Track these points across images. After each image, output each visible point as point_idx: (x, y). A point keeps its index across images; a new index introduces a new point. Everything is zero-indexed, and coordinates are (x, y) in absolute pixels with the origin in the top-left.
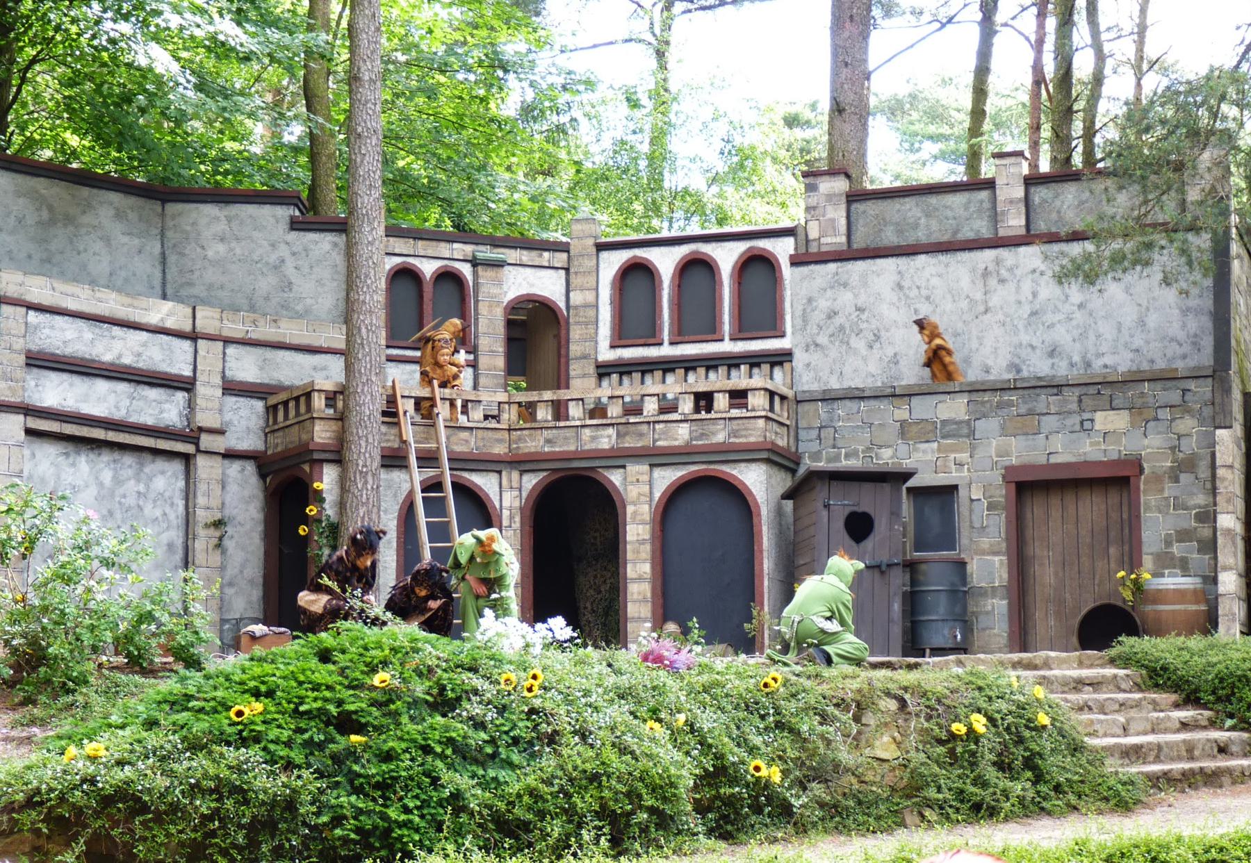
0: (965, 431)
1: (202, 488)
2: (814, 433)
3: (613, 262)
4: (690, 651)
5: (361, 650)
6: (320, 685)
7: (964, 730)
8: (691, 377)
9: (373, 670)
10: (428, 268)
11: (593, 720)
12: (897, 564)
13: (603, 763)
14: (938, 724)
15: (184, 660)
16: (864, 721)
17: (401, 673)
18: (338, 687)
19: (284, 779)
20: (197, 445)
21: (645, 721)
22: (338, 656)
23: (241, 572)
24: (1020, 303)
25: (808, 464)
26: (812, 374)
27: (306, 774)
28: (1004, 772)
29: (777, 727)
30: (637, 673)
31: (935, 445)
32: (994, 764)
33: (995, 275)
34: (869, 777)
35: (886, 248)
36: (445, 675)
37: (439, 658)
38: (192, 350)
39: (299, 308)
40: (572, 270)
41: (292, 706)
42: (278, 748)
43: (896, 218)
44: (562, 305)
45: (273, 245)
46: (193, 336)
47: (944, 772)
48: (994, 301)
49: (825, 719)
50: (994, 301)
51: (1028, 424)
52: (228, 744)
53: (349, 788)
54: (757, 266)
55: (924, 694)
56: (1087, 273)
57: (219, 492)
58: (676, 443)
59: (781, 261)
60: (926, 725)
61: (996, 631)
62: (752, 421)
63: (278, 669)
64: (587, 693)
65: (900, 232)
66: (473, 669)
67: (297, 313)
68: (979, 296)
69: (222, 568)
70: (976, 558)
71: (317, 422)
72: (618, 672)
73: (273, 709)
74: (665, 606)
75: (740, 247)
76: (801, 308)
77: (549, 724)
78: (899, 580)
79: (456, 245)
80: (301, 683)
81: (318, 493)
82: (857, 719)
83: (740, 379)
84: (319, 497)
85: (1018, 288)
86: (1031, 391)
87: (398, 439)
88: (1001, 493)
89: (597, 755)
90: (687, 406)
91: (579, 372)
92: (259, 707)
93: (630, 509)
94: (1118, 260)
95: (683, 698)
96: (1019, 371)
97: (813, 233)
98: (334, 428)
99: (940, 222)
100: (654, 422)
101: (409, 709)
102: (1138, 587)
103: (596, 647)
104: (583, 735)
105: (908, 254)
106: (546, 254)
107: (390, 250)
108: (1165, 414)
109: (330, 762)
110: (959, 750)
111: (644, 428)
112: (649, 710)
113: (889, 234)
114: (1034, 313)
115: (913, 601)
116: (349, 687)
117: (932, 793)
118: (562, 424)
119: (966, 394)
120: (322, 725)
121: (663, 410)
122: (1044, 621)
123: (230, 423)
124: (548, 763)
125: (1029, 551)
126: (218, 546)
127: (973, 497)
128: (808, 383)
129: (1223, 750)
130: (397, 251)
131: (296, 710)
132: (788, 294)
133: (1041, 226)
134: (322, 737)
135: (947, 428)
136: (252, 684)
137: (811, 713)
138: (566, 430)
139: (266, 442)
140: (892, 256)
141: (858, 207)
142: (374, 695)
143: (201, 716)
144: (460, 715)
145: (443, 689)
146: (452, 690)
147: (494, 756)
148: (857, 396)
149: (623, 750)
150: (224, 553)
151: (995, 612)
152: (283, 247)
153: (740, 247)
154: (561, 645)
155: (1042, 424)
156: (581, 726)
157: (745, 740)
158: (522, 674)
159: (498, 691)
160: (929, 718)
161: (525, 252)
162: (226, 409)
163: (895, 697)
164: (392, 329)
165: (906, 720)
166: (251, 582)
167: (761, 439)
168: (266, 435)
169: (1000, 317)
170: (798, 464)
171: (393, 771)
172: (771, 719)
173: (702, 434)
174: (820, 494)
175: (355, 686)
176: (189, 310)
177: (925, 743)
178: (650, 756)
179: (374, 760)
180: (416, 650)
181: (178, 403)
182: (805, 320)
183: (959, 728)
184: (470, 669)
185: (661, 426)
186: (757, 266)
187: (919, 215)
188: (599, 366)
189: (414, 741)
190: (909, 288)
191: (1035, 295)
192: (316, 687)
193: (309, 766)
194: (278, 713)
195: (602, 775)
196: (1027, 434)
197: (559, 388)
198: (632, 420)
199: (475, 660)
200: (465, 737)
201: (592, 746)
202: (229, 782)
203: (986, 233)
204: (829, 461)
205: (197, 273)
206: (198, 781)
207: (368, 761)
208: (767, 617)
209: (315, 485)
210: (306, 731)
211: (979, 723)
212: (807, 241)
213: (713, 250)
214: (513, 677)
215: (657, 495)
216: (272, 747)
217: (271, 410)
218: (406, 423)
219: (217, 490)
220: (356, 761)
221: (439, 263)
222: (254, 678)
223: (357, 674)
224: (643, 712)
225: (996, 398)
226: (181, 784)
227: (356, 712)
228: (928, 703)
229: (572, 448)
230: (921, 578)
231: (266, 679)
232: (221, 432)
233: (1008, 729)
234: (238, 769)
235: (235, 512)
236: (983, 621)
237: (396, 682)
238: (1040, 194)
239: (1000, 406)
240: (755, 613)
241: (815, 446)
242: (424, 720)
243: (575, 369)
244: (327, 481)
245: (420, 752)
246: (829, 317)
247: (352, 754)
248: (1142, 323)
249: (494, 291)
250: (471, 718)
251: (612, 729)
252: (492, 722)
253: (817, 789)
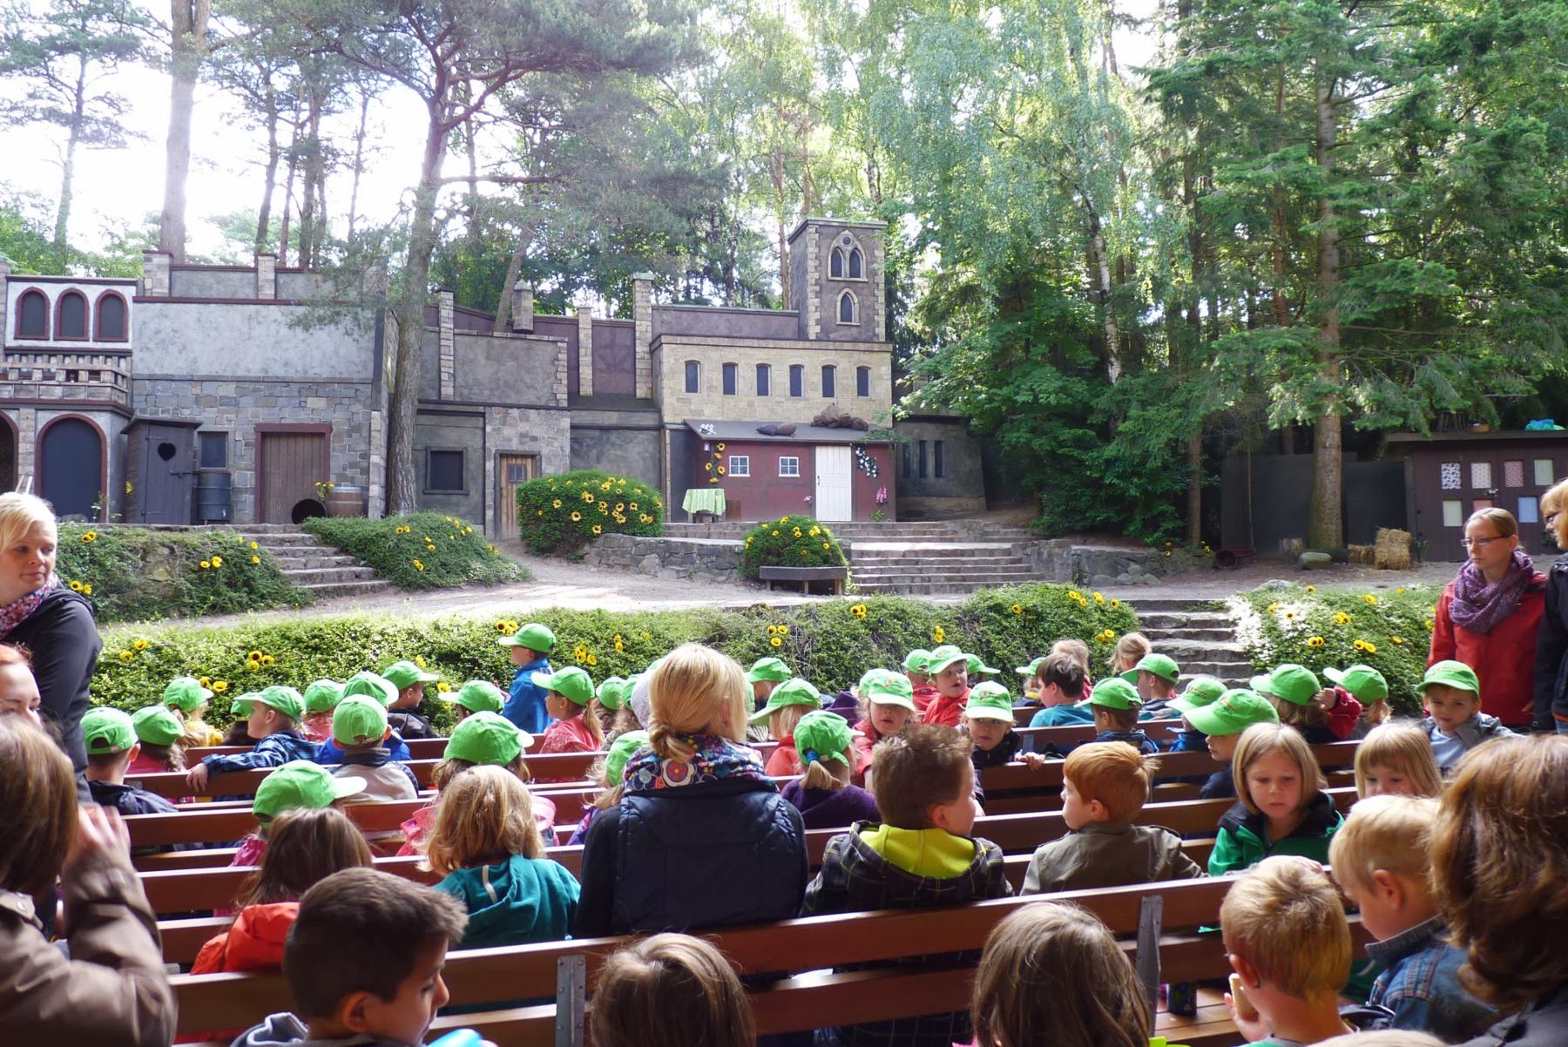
3: (16, 290)
8: (67, 360)
25: (138, 414)
34: (150, 590)
49: (122, 558)
50: (255, 333)
54: (111, 301)
56: (304, 324)
65: (201, 290)
68: (245, 330)
75: (102, 289)
78: (190, 481)
82: (143, 559)
83: (98, 364)
88: (252, 438)
90: (61, 377)
93: (21, 434)
94: (321, 320)
97: (148, 285)
102: (327, 490)
108: (346, 401)
114: (277, 342)
115: (198, 494)
117: (187, 600)
121: (45, 378)
122: (276, 507)
125: (268, 469)
128: (141, 369)
129: (358, 576)
132: (131, 318)
133: (283, 296)
141: (176, 274)
148: (170, 379)
153: (102, 289)
174: (144, 432)
183: (205, 564)
186: (111, 301)
188: (6, 349)
203: (252, 296)
211: (217, 562)
215: (40, 427)
225: (252, 386)
236: (240, 506)
238: (283, 278)
241: (143, 405)
248: (336, 352)
253: (114, 598)
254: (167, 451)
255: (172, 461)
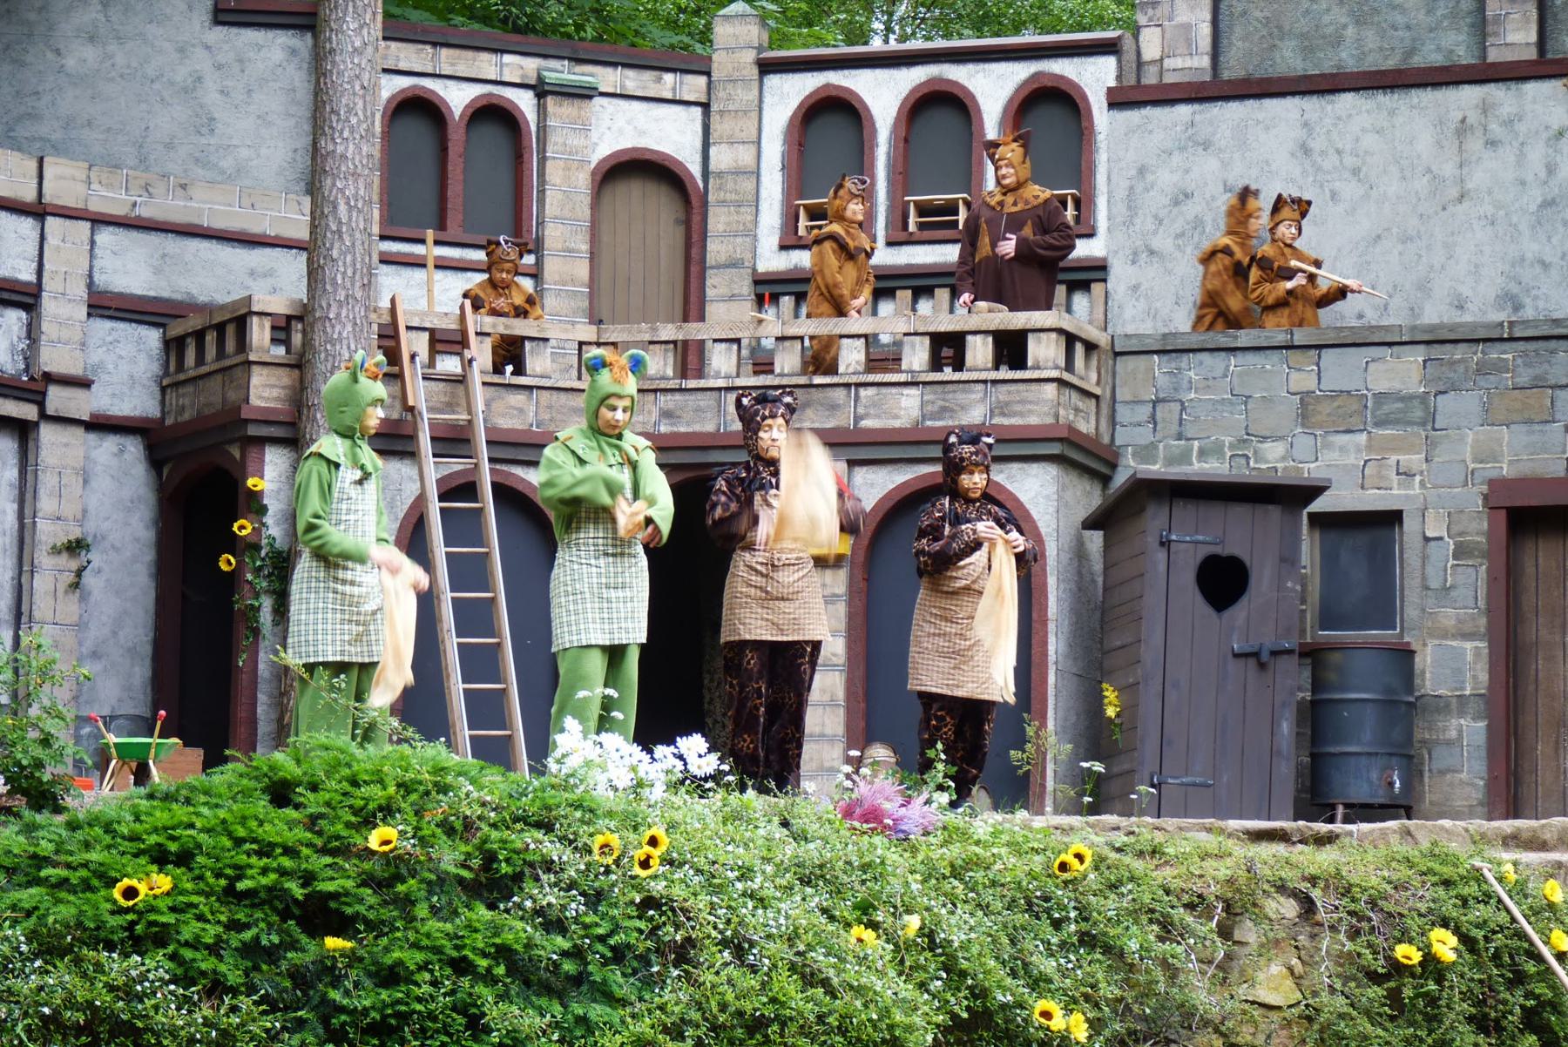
0: (1418, 413)
1: (47, 482)
2: (1144, 412)
4: (928, 802)
5: (346, 786)
6: (272, 845)
7: (1417, 957)
8: (924, 306)
9: (368, 822)
10: (458, 98)
11: (756, 921)
12: (1289, 652)
13: (773, 1000)
14: (1370, 945)
15: (25, 793)
16: (1237, 936)
17: (417, 829)
18: (305, 851)
19: (208, 1012)
20: (41, 405)
21: (848, 925)
22: (303, 794)
23: (115, 633)
24: (1523, 183)
25: (1130, 467)
26: (1142, 305)
27: (245, 1003)
28: (1488, 1035)
29: (1081, 942)
30: (833, 838)
31: (1363, 437)
32: (1470, 1019)
33: (1479, 132)
35: (1281, 80)
36: (495, 835)
37: (484, 804)
38: (35, 235)
39: (227, 163)
40: (714, 107)
41: (223, 882)
42: (198, 956)
43: (1303, 25)
44: (695, 169)
45: (181, 50)
46: (38, 211)
47: (1380, 1032)
48: (1478, 178)
49: (1168, 929)
50: (1478, 178)
51: (1534, 403)
52: (110, 946)
53: (321, 1031)
55: (1347, 891)
57: (79, 491)
58: (897, 424)
59: (1092, 99)
60: (1349, 946)
61: (1464, 776)
62: (1034, 386)
63: (198, 814)
64: (746, 873)
65: (1307, 51)
66: (546, 826)
67: (223, 172)
68: (1449, 169)
69: (80, 626)
70: (1431, 643)
71: (255, 369)
72: (801, 837)
73: (189, 886)
74: (869, 716)
76: (1125, 184)
77: (677, 927)
78: (1295, 682)
79: (507, 58)
80: (239, 842)
81: (255, 497)
82: (1225, 932)
84: (254, 505)
85: (1521, 157)
86: (1541, 344)
87: (398, 405)
88: (1478, 527)
89: (763, 984)
90: (917, 357)
91: (723, 291)
92: (164, 882)
95: (915, 887)
96: (1517, 307)
98: (286, 381)
99: (1382, 34)
100: (859, 385)
101: (431, 893)
103: (763, 790)
104: (739, 948)
105: (1321, 92)
106: (669, 78)
107: (390, 65)
109: (288, 984)
110: (1408, 992)
111: (840, 394)
112: (855, 907)
113: (1288, 54)
114: (1548, 204)
115: (1317, 719)
116: (324, 851)
118: (692, 384)
119: (1422, 348)
120: (275, 918)
121: (873, 364)
123: (97, 368)
124: (675, 997)
126: (75, 586)
127: (1429, 534)
130: (403, 66)
131: (230, 891)
132: (1102, 159)
134: (275, 939)
135: (1386, 408)
136: (153, 839)
137: (1144, 919)
138: (699, 395)
139: (163, 402)
140: (1293, 94)
142: (367, 866)
143: (63, 895)
144: (519, 906)
145: (490, 858)
146: (507, 860)
147: (578, 980)
149: (810, 978)
150: (84, 599)
151: (1463, 741)
152: (200, 53)
154: (699, 786)
155: (1558, 404)
156: (735, 931)
157: (1026, 965)
158: (632, 836)
159: (588, 865)
160: (1354, 934)
161: (631, 73)
162: (92, 342)
163: (1295, 894)
164: (389, 205)
165: (1313, 936)
166: (132, 651)
167: (1050, 420)
168: (163, 390)
169: (1488, 209)
170: (1114, 466)
171: (399, 1002)
172: (1073, 927)
173: (944, 409)
174: (1155, 520)
175: (339, 850)
176: (34, 165)
177: (1346, 979)
178: (859, 991)
179: (368, 983)
180: (443, 789)
181: (9, 331)
182: (1132, 208)
183: (1408, 953)
184: (538, 825)
185: (871, 391)
187: (1343, 20)
188: (760, 281)
189: (437, 950)
190: (1323, 153)
191: (1551, 169)
192: (266, 850)
193: (251, 989)
194: (198, 893)
195: (770, 1021)
196: (1529, 422)
197: (686, 319)
198: (818, 380)
199: (549, 808)
200: (529, 946)
201: (754, 969)
202: (113, 1016)
203: (1464, 55)
204: (1170, 461)
205: (46, 99)
206: (56, 1012)
207: (356, 985)
208: (1052, 739)
209: (250, 482)
210: (247, 926)
211: (1445, 945)
212: (1140, 64)
213: (970, 76)
214: (615, 840)
216: (188, 954)
217: (175, 346)
218: (414, 374)
219: (74, 485)
220: (336, 983)
221: (476, 90)
222: (156, 830)
223: (339, 828)
224: (844, 909)
225: (1476, 355)
226: (26, 1015)
227: (335, 896)
228: (1352, 907)
229: (709, 427)
230: (1332, 677)
231: (178, 832)
232: (84, 384)
233: (1496, 957)
234: (126, 992)
235: (106, 525)
236: (1442, 758)
237: (408, 845)
239: (1482, 370)
240: (1030, 731)
241: (1144, 435)
242: (456, 913)
243: (716, 285)
244: (270, 475)
245: (448, 971)
246: (1176, 203)
247: (328, 970)
249: (575, 141)
250: (539, 912)
251: (791, 940)
252: (576, 920)
254: (1223, 581)
255: (1239, 613)
